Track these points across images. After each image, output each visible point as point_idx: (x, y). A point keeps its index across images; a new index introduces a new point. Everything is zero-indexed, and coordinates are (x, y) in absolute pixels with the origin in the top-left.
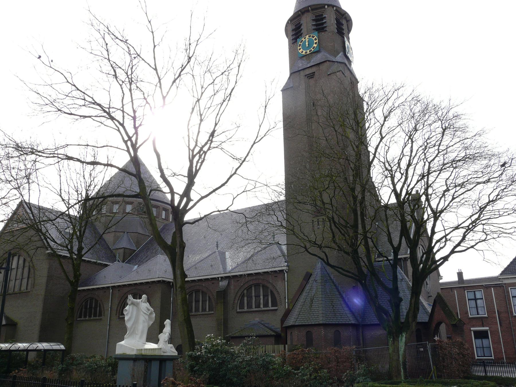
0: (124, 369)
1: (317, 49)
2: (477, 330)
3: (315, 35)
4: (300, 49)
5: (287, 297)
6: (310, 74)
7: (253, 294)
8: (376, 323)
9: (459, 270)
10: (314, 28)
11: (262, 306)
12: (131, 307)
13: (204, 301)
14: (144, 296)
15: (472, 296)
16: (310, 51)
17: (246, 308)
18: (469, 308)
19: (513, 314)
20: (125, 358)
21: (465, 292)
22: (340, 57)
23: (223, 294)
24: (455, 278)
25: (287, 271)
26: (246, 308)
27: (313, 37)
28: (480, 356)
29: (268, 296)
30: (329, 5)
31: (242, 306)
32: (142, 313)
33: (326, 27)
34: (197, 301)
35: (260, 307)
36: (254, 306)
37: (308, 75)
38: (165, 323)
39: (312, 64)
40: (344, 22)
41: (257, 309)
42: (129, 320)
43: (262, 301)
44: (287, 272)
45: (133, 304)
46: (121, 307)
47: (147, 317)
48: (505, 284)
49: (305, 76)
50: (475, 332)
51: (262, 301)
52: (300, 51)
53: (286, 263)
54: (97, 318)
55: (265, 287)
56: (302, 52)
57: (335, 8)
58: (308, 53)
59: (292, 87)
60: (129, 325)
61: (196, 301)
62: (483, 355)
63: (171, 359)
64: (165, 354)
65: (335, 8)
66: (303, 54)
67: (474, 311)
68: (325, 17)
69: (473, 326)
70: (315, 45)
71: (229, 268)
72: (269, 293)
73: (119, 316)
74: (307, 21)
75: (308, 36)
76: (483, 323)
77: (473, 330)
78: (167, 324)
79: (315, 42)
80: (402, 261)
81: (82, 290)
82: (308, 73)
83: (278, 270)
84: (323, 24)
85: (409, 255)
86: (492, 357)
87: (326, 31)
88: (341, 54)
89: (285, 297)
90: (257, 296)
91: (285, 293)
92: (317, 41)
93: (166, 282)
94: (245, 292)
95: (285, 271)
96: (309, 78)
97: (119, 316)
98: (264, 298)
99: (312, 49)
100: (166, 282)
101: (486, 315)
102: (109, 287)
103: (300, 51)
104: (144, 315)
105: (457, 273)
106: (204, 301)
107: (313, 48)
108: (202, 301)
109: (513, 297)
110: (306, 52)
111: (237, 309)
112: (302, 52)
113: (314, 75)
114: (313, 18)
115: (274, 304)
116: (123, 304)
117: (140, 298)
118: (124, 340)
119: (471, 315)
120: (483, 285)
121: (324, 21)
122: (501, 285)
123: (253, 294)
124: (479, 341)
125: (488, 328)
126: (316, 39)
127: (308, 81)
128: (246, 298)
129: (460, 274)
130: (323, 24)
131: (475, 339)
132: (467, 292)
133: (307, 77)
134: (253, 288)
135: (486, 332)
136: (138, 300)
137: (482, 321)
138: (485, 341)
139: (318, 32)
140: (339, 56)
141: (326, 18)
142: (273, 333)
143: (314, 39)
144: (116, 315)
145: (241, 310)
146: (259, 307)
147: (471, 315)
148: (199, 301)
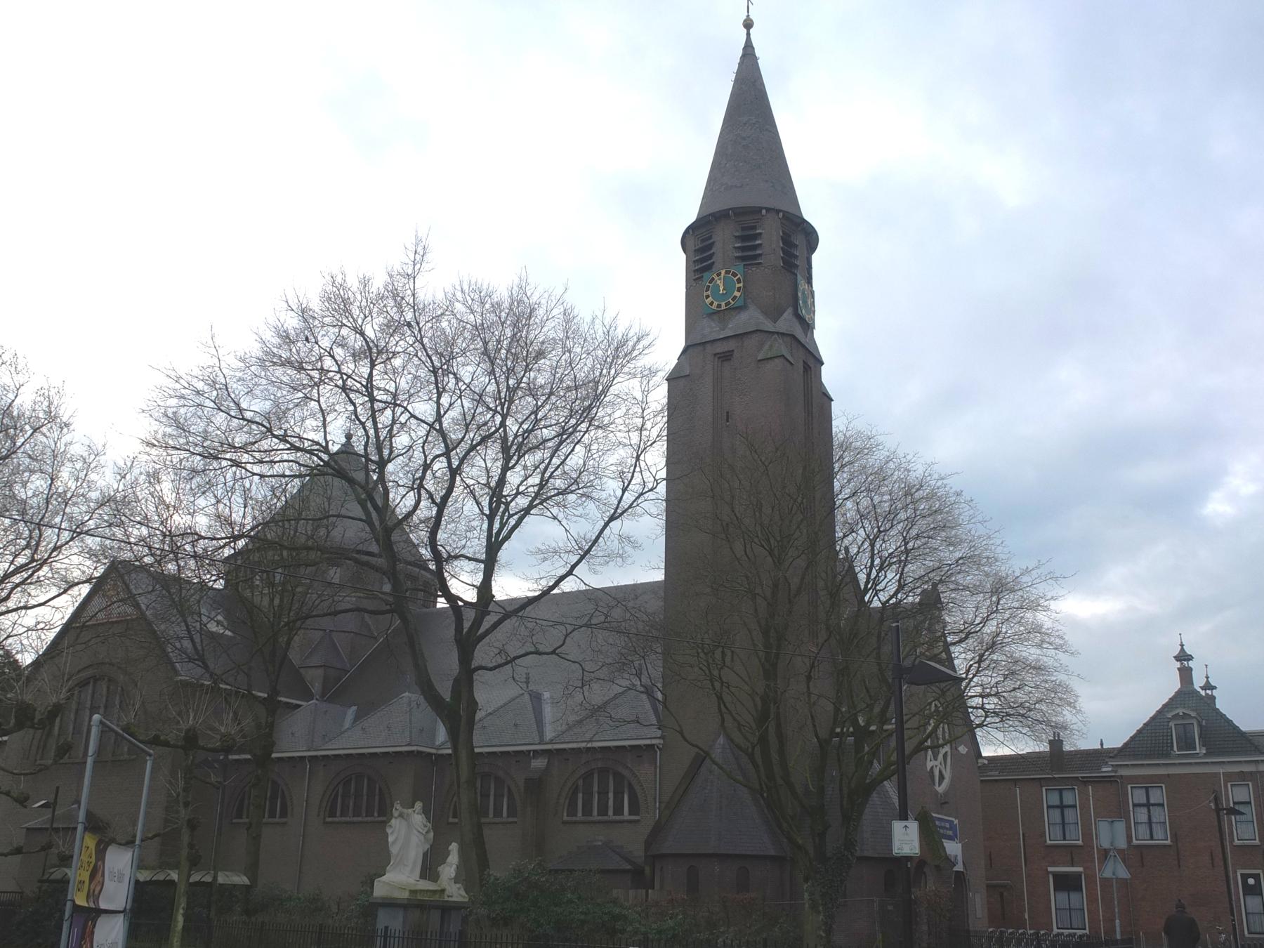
0: (384, 920)
1: (740, 303)
2: (1067, 872)
3: (739, 269)
4: (707, 297)
5: (659, 798)
7: (596, 789)
10: (737, 255)
11: (611, 812)
12: (398, 821)
13: (498, 797)
15: (1054, 799)
17: (580, 814)
20: (390, 904)
21: (1042, 792)
22: (786, 322)
23: (536, 785)
25: (661, 746)
26: (580, 814)
29: (623, 793)
30: (768, 210)
31: (572, 811)
32: (415, 831)
36: (595, 812)
37: (721, 353)
38: (450, 848)
40: (799, 240)
41: (600, 818)
42: (394, 842)
43: (611, 803)
45: (401, 815)
46: (328, 802)
47: (422, 838)
49: (715, 355)
50: (1057, 876)
51: (611, 803)
52: (707, 301)
53: (660, 732)
54: (277, 820)
55: (619, 777)
56: (712, 303)
57: (781, 215)
58: (723, 307)
59: (688, 375)
60: (394, 850)
62: (1069, 927)
63: (458, 907)
64: (450, 899)
65: (781, 215)
66: (713, 307)
67: (1058, 831)
69: (1054, 865)
70: (737, 294)
71: (549, 734)
72: (626, 790)
73: (324, 818)
75: (724, 270)
76: (1072, 859)
77: (1051, 872)
78: (453, 849)
79: (737, 286)
82: (721, 351)
83: (644, 745)
84: (755, 247)
85: (894, 726)
88: (788, 314)
89: (655, 798)
90: (603, 793)
91: (656, 790)
92: (741, 285)
93: (424, 754)
94: (580, 782)
95: (658, 747)
97: (324, 818)
98: (615, 797)
100: (424, 754)
101: (1080, 842)
102: (305, 757)
103: (708, 301)
106: (498, 797)
107: (733, 300)
109: (1135, 805)
110: (719, 306)
111: (563, 815)
112: (712, 303)
113: (732, 355)
115: (634, 809)
123: (596, 789)
124: (1063, 896)
125: (1081, 869)
126: (739, 281)
127: (720, 364)
128: (580, 795)
130: (755, 247)
131: (1054, 890)
132: (1046, 789)
133: (719, 358)
134: (596, 776)
135: (1079, 875)
138: (1074, 897)
140: (782, 318)
142: (629, 867)
143: (735, 279)
144: (318, 815)
145: (569, 819)
147: (1050, 840)
148: (489, 796)
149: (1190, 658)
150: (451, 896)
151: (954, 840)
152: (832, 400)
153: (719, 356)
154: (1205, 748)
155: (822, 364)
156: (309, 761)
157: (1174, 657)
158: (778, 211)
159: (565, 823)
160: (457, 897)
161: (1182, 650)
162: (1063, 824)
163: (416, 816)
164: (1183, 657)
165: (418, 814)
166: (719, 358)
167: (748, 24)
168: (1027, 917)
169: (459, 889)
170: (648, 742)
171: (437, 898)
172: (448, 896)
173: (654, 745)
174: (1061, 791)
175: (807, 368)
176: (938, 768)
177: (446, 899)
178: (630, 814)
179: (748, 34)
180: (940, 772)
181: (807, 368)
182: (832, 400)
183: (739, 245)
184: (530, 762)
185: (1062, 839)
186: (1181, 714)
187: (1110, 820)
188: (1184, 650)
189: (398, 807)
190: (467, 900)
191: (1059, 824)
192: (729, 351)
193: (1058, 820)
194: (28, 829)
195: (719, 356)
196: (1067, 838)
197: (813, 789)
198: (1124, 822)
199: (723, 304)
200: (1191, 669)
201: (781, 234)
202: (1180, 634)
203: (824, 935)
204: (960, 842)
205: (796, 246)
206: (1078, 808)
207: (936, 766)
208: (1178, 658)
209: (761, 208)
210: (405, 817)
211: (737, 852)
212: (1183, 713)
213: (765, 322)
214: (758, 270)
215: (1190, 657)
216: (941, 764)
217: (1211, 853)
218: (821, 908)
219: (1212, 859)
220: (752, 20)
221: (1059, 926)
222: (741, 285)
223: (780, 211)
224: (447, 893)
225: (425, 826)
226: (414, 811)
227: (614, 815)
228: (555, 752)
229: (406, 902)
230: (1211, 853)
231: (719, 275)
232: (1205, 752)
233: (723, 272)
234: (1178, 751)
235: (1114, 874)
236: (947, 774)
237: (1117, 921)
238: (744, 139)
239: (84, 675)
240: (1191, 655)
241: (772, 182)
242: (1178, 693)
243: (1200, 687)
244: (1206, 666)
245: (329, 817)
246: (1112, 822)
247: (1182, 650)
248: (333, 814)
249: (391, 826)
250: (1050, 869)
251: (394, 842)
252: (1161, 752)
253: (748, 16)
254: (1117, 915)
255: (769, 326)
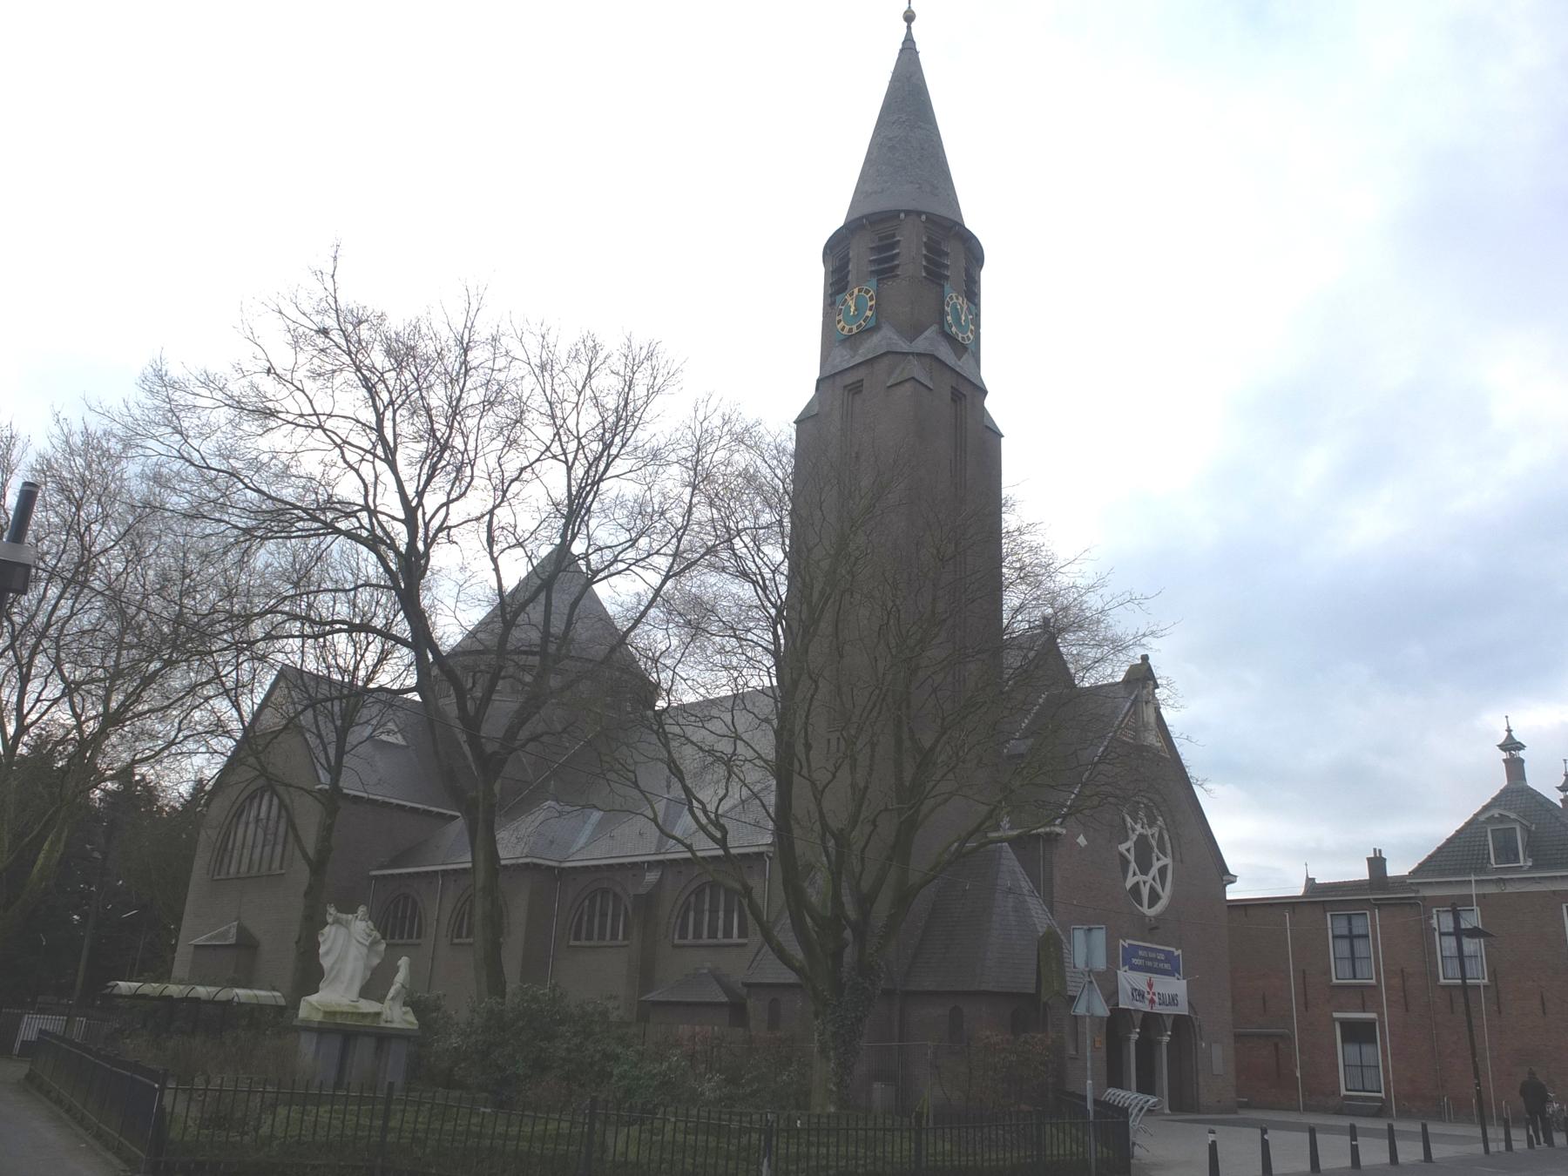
1: (872, 323)
2: (1365, 1019)
4: (839, 322)
6: (853, 383)
7: (707, 906)
8: (791, 981)
9: (1375, 850)
10: (873, 269)
11: (720, 935)
12: (334, 928)
14: (362, 910)
16: (858, 327)
18: (1335, 958)
19: (1439, 980)
23: (647, 903)
24: (1361, 873)
25: (771, 855)
27: (867, 292)
28: (1370, 1089)
30: (908, 213)
31: (683, 936)
32: (354, 941)
33: (897, 266)
34: (604, 915)
35: (716, 938)
38: (400, 962)
39: (858, 359)
42: (327, 953)
44: (770, 858)
45: (337, 921)
47: (365, 951)
48: (1424, 898)
49: (845, 387)
50: (1345, 1024)
56: (843, 329)
57: (924, 217)
58: (855, 331)
60: (326, 963)
61: (710, 912)
62: (1361, 1088)
63: (401, 1035)
64: (388, 1025)
65: (924, 217)
68: (899, 241)
70: (869, 313)
73: (452, 940)
74: (861, 254)
77: (1338, 1019)
79: (870, 304)
80: (1041, 840)
81: (604, 865)
82: (851, 382)
86: (1380, 1092)
87: (897, 276)
90: (714, 911)
92: (873, 302)
94: (693, 899)
96: (853, 395)
97: (452, 940)
99: (862, 321)
103: (839, 326)
104: (357, 944)
105: (1369, 859)
108: (613, 915)
110: (851, 330)
111: (673, 938)
112: (843, 329)
113: (862, 385)
114: (873, 245)
116: (579, 913)
117: (354, 911)
118: (317, 992)
119: (1337, 979)
120: (1369, 899)
121: (894, 252)
122: (1412, 901)
123: (707, 906)
124: (1353, 1049)
129: (1377, 863)
131: (1343, 1042)
132: (1331, 915)
134: (708, 891)
136: (350, 916)
137: (1364, 996)
138: (1367, 1049)
139: (878, 280)
140: (923, 336)
141: (901, 243)
143: (868, 296)
146: (700, 937)
148: (607, 915)
149: (1520, 747)
150: (391, 1022)
151: (1174, 976)
152: (1003, 436)
153: (849, 388)
154: (1530, 859)
155: (985, 392)
156: (442, 876)
157: (1499, 746)
158: (919, 213)
159: (675, 946)
160: (400, 1022)
161: (1510, 736)
162: (1353, 958)
163: (358, 923)
164: (1511, 745)
165: (361, 920)
166: (850, 390)
167: (909, 17)
168: (1298, 1075)
169: (405, 1013)
170: (756, 850)
171: (367, 1022)
172: (386, 1022)
173: (763, 853)
174: (1349, 917)
175: (957, 396)
176: (1148, 885)
177: (383, 1024)
178: (739, 937)
179: (909, 28)
180: (1152, 889)
181: (957, 396)
182: (1003, 436)
183: (874, 257)
184: (645, 876)
185: (1352, 976)
186: (1497, 816)
187: (1085, 927)
188: (1513, 738)
189: (332, 910)
190: (416, 1027)
191: (1348, 958)
192: (859, 381)
193: (1347, 953)
194: (197, 947)
195: (849, 388)
196: (1358, 976)
197: (66, 830)
198: (1104, 931)
199: (854, 327)
200: (1522, 761)
201: (925, 239)
202: (1507, 717)
203: (834, 1089)
204: (1184, 979)
205: (947, 254)
206: (1370, 938)
207: (1145, 883)
208: (1503, 747)
209: (900, 211)
210: (344, 923)
211: (782, 981)
212: (1501, 815)
213: (900, 342)
214: (894, 284)
215: (1519, 745)
216: (1154, 879)
217: (1542, 997)
218: (832, 1053)
219: (1543, 1004)
220: (913, 12)
221: (1349, 1088)
222: (873, 302)
223: (924, 213)
224: (384, 1017)
225: (369, 936)
226: (357, 917)
227: (724, 937)
228: (710, 860)
229: (316, 1025)
230: (1542, 997)
231: (851, 295)
232: (1530, 864)
233: (856, 291)
234: (1496, 864)
235: (1088, 1010)
236: (1165, 895)
237: (1089, 1082)
238: (890, 139)
239: (252, 787)
240: (1519, 743)
241: (919, 184)
242: (1504, 792)
243: (1557, 788)
244: (1565, 760)
245: (457, 938)
246: (1090, 930)
247: (1510, 736)
248: (459, 936)
249: (323, 934)
250: (1336, 1015)
251: (327, 953)
252: (1473, 866)
253: (909, 7)
254: (1089, 1073)
255: (904, 346)
